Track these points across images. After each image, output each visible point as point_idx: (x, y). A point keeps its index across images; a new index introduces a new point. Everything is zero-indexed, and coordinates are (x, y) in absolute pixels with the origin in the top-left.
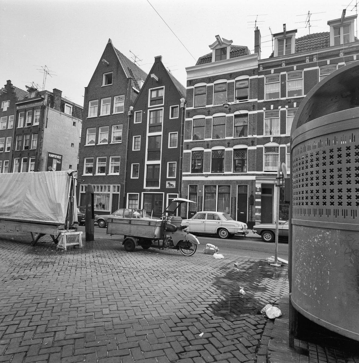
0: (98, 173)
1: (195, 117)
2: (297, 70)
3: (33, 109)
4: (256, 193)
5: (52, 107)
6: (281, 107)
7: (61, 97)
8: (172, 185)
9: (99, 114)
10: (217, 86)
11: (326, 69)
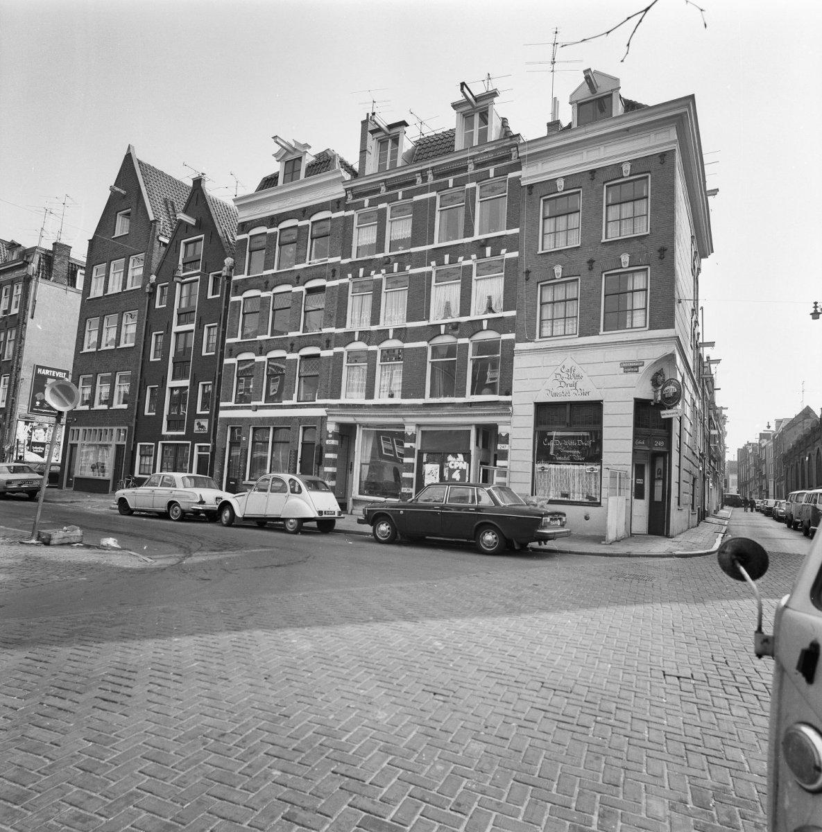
0: (119, 403)
1: (277, 290)
2: (403, 199)
3: (12, 282)
4: (328, 442)
5: (47, 276)
6: (374, 271)
7: (69, 258)
8: (203, 427)
9: (106, 290)
10: (284, 233)
11: (449, 197)
